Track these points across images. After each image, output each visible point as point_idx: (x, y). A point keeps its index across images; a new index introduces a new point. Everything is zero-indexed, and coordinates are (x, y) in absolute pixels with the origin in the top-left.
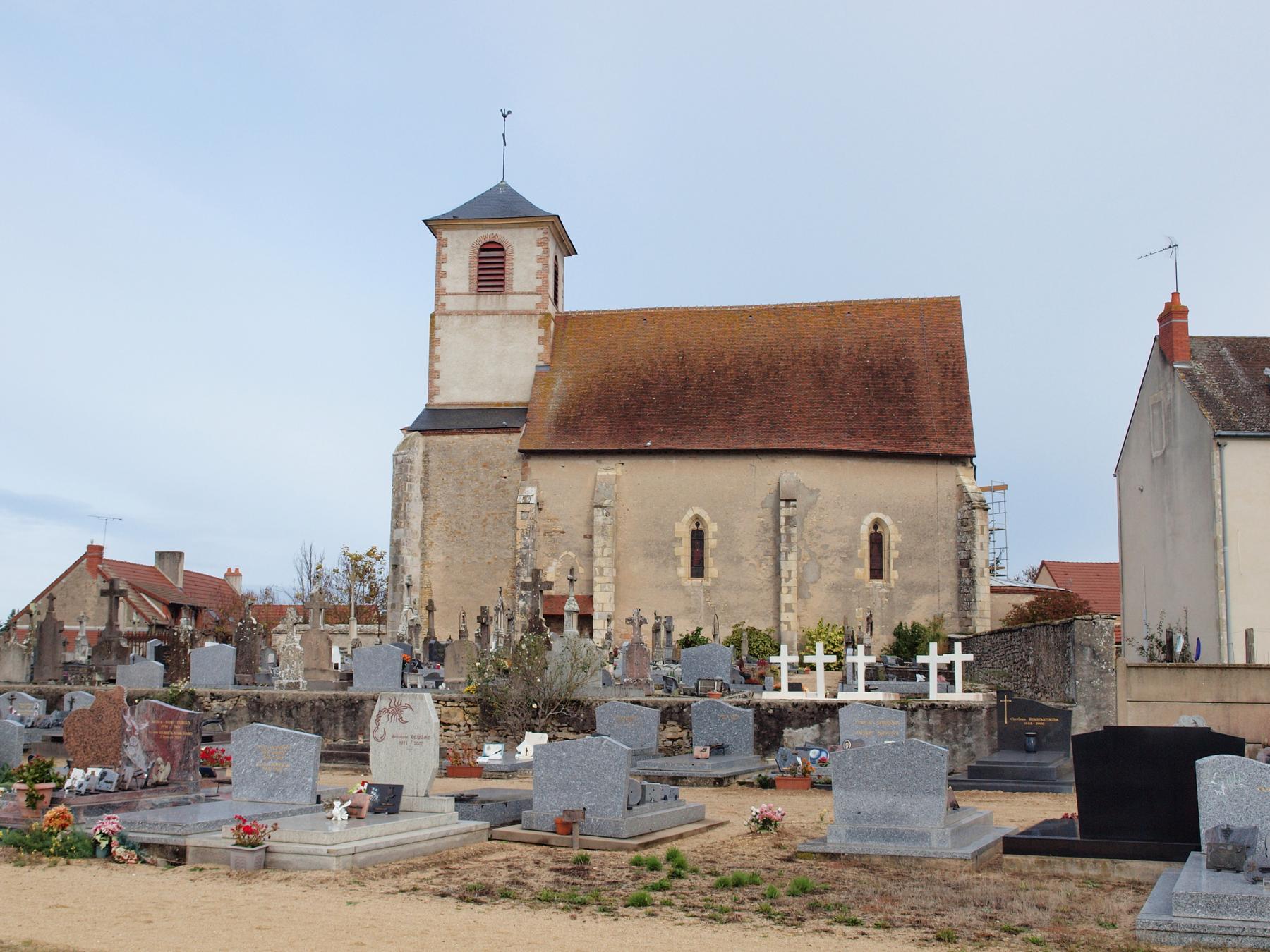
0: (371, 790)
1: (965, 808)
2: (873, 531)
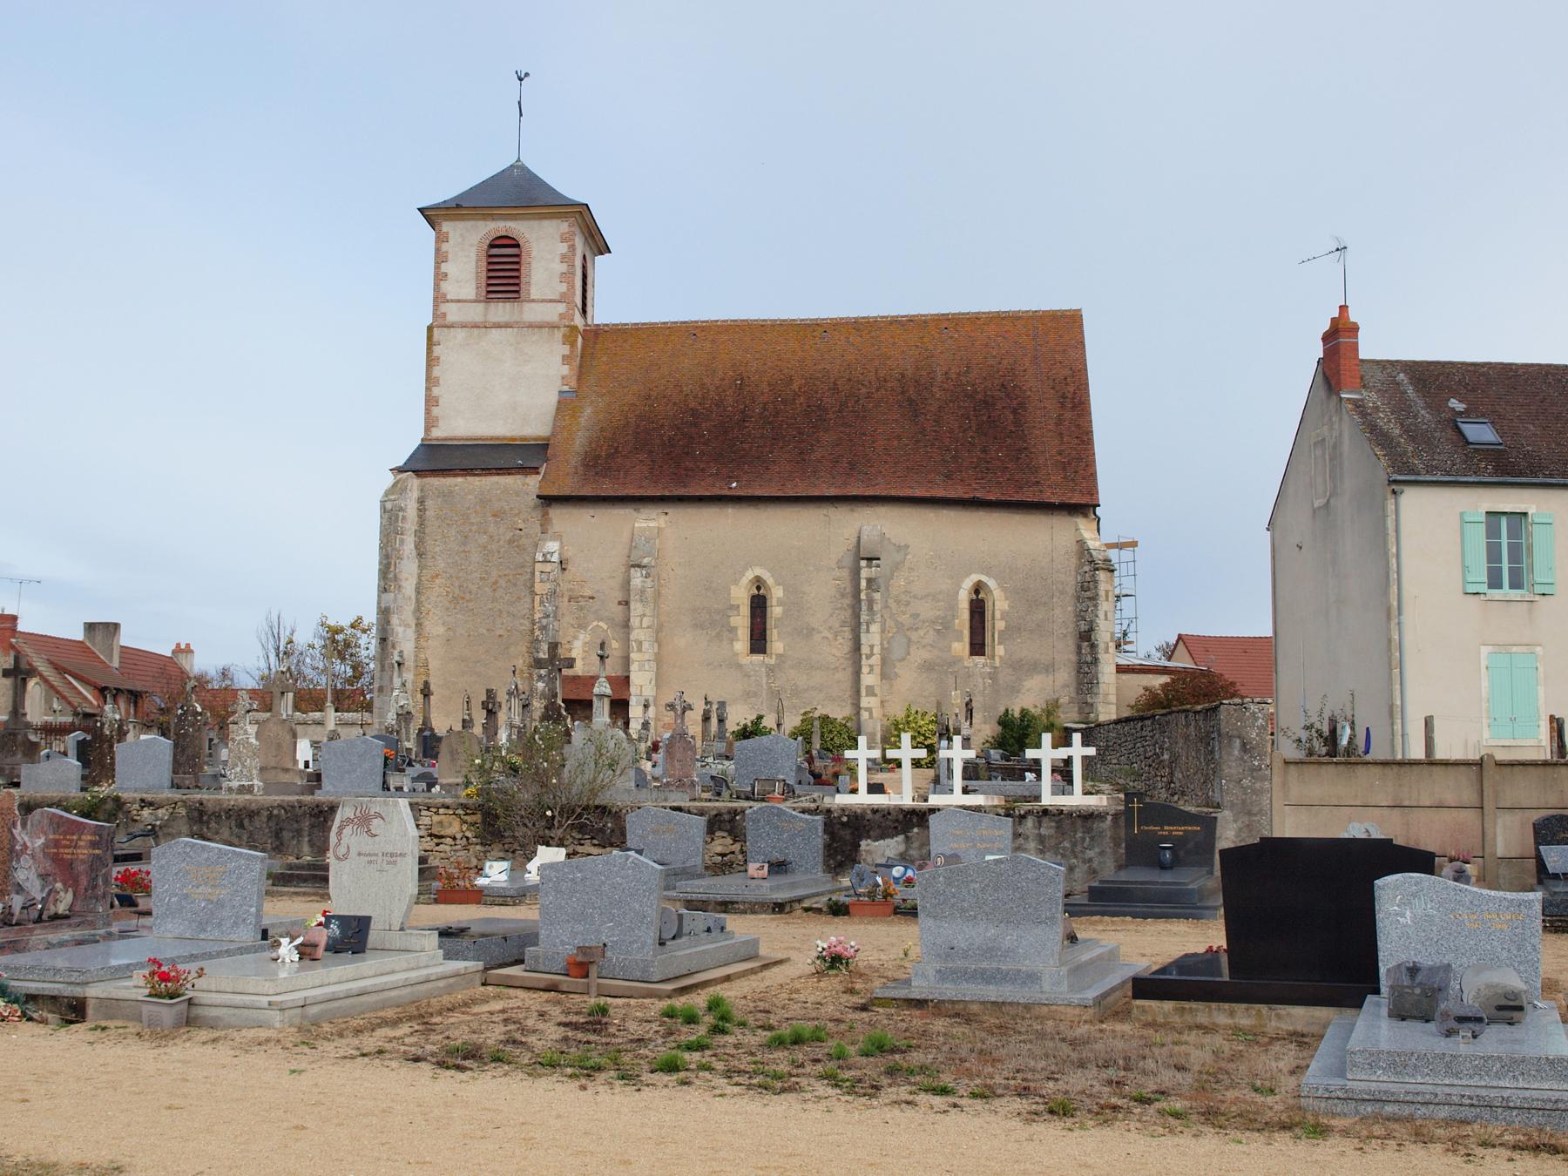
0: (330, 923)
1: (1086, 941)
2: (974, 597)
